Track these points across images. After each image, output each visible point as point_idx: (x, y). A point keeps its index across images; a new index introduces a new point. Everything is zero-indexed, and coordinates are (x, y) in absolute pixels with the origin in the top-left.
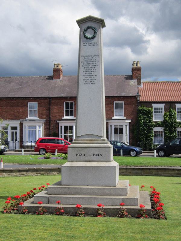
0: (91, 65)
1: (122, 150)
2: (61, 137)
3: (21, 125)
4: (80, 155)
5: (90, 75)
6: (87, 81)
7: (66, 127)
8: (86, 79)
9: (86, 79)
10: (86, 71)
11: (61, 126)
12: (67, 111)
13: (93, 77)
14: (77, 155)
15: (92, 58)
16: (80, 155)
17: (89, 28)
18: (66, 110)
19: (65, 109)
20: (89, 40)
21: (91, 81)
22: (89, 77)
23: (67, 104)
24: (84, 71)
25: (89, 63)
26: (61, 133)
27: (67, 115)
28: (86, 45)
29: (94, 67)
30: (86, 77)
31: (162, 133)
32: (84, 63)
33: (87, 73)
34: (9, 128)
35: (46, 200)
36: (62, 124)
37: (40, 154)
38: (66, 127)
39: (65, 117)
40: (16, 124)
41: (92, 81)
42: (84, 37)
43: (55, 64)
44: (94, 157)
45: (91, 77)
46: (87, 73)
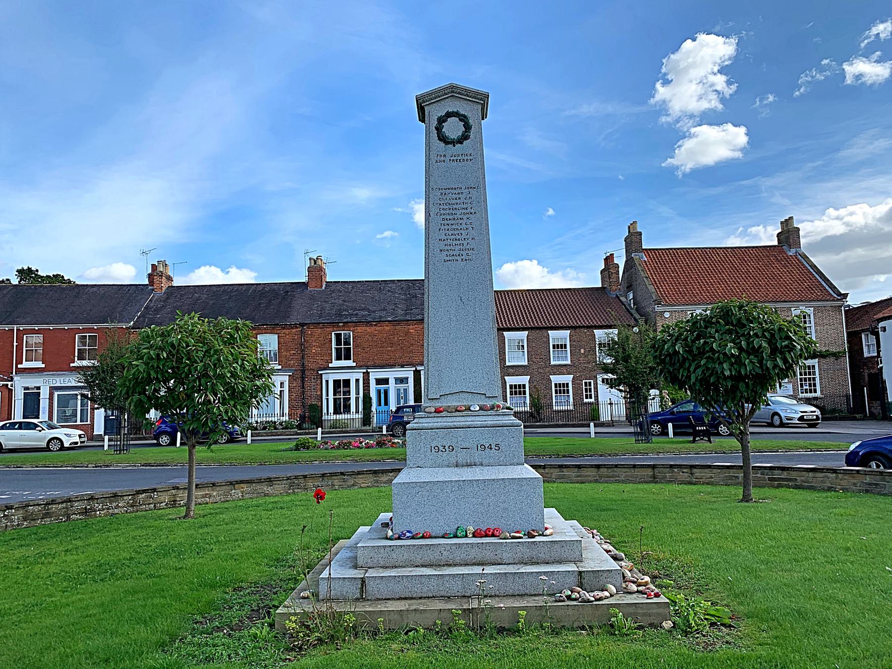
0: (459, 212)
1: (670, 425)
2: (751, 426)
3: (417, 374)
4: (441, 448)
5: (458, 237)
6: (451, 253)
7: (337, 383)
8: (449, 248)
9: (449, 248)
10: (446, 227)
11: (327, 382)
12: (338, 351)
13: (465, 243)
14: (433, 450)
15: (462, 193)
16: (441, 448)
17: (449, 115)
18: (337, 349)
19: (334, 346)
20: (451, 146)
21: (461, 252)
22: (454, 242)
23: (338, 336)
24: (443, 227)
25: (454, 207)
26: (357, 399)
27: (339, 358)
28: (444, 161)
29: (467, 216)
30: (449, 242)
31: (568, 386)
32: (442, 207)
33: (451, 232)
34: (392, 381)
35: (353, 591)
36: (330, 377)
37: (158, 445)
38: (337, 383)
39: (335, 363)
40: (408, 373)
41: (464, 253)
42: (440, 139)
43: (39, 388)
44: (480, 452)
45: (461, 242)
46: (451, 232)
